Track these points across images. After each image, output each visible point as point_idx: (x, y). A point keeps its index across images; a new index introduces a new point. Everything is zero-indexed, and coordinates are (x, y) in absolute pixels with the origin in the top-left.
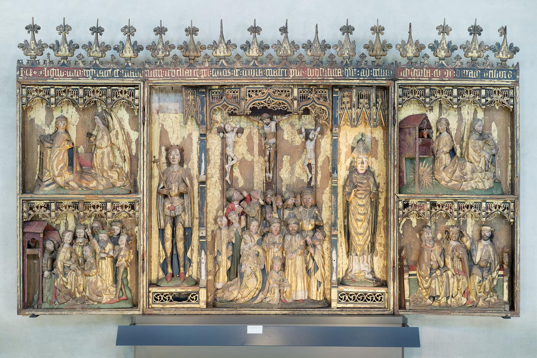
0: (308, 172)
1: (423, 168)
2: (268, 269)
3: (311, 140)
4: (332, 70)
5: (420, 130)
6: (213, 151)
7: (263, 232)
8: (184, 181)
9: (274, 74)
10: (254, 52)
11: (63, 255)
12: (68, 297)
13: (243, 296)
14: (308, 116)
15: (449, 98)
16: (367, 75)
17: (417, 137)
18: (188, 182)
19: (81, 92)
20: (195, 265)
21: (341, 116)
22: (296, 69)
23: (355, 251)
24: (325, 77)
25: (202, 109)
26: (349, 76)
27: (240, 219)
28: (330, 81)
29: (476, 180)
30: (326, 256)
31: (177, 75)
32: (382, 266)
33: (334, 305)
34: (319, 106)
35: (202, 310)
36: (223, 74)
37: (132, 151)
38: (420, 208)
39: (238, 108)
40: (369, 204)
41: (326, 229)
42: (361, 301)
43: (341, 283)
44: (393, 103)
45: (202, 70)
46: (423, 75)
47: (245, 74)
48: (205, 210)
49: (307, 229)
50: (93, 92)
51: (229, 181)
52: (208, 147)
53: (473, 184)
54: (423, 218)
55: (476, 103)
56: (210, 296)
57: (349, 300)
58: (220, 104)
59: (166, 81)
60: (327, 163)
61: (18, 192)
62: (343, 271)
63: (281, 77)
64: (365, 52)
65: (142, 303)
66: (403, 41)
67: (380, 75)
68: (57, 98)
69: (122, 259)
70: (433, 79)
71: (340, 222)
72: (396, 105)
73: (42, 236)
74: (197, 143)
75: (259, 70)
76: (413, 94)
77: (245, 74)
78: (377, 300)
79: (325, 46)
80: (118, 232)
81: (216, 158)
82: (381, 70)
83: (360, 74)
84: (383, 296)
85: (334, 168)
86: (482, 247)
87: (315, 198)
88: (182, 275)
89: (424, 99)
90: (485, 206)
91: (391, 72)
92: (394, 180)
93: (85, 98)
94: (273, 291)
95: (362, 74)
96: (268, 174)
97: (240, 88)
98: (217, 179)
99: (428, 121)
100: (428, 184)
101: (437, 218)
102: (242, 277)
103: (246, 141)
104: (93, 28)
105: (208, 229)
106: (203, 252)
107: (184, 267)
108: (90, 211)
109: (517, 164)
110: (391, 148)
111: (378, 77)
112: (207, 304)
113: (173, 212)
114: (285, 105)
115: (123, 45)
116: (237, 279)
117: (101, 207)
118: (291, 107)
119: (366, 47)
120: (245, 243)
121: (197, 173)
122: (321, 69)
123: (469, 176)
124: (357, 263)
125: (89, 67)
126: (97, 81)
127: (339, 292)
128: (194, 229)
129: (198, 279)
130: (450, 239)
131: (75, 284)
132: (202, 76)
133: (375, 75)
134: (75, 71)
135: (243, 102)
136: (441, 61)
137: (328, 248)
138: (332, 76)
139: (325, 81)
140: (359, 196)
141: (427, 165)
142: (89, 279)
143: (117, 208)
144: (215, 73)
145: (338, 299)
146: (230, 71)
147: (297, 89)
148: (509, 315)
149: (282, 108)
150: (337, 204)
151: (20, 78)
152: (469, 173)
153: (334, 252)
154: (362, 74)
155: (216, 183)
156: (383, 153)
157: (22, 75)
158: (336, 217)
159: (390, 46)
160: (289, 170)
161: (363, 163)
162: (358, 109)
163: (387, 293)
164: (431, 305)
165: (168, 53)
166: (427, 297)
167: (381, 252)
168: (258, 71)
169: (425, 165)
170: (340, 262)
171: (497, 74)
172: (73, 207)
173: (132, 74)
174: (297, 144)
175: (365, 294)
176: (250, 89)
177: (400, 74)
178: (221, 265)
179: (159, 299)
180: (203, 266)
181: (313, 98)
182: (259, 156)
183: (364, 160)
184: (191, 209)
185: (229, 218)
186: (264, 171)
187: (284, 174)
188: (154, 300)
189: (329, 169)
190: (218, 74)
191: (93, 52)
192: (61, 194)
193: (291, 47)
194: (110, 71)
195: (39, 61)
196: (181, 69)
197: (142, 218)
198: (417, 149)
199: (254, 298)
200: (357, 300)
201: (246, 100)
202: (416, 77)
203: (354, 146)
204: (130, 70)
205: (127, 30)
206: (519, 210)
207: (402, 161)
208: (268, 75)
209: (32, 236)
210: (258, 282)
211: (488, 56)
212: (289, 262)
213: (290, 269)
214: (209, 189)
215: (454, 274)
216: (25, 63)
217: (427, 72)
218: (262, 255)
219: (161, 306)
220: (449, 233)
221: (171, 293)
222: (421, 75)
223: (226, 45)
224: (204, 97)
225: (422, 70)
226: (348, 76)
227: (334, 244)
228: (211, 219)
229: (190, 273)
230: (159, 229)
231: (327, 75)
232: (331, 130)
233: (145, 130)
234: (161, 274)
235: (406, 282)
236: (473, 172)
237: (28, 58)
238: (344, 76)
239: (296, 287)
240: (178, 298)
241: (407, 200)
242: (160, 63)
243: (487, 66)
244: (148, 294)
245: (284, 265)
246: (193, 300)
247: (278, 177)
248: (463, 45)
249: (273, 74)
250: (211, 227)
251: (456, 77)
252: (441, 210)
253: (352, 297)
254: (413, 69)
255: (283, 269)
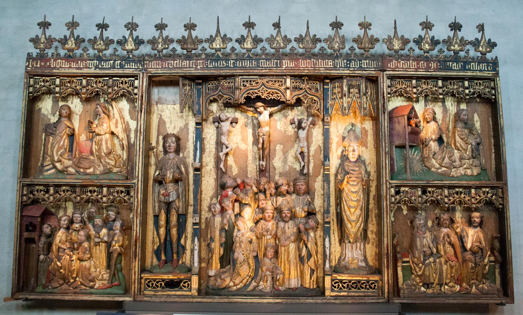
0: (301, 160)
1: (412, 156)
2: (261, 256)
3: (304, 129)
4: (323, 61)
5: (409, 119)
6: (208, 140)
7: (256, 218)
8: (179, 168)
9: (268, 64)
10: (248, 45)
11: (61, 235)
12: (61, 282)
13: (236, 284)
14: (300, 107)
15: (434, 89)
16: (357, 66)
17: (406, 125)
18: (183, 169)
19: (84, 82)
20: (188, 252)
21: (332, 106)
22: (289, 60)
23: (348, 238)
24: (317, 67)
25: (199, 100)
26: (340, 67)
27: (234, 206)
28: (322, 71)
29: (465, 166)
30: (319, 244)
31: (175, 66)
32: (374, 253)
33: (328, 293)
34: (310, 96)
35: (193, 298)
36: (219, 65)
37: (130, 139)
38: (411, 195)
39: (233, 97)
40: (361, 191)
41: (319, 217)
42: (355, 288)
43: (336, 270)
44: (382, 92)
45: (199, 61)
46: (410, 66)
47: (239, 65)
48: (199, 197)
49: (300, 216)
50: (96, 82)
51: (223, 169)
52: (204, 136)
53: (461, 171)
54: (414, 205)
55: (460, 94)
56: (203, 283)
57: (342, 288)
58: (216, 94)
59: (164, 71)
60: (319, 152)
61: (19, 176)
62: (335, 259)
63: (274, 67)
64: (355, 46)
65: (133, 289)
66: (389, 36)
67: (369, 66)
68: (62, 88)
69: (116, 244)
70: (419, 70)
71: (333, 209)
72: (385, 95)
73: (39, 219)
74: (193, 132)
75: (253, 61)
76: (401, 85)
77: (239, 65)
78: (371, 288)
79: (316, 40)
80: (113, 217)
81: (211, 147)
82: (370, 61)
83: (350, 65)
84: (376, 284)
85: (326, 156)
86: (473, 233)
87: (307, 184)
88: (175, 262)
89: (411, 89)
90: (474, 192)
91: (380, 63)
92: (386, 166)
93: (87, 88)
94: (265, 280)
95: (352, 65)
96: (261, 162)
97: (234, 79)
98: (212, 167)
99: (415, 111)
100: (419, 171)
101: (428, 204)
102: (234, 265)
103: (240, 130)
104: (99, 25)
105: (202, 217)
106: (196, 239)
107: (178, 253)
108: (87, 195)
109: (503, 151)
110: (382, 135)
111: (367, 68)
112: (199, 291)
113: (167, 198)
114: (279, 95)
115: (126, 38)
116: (229, 266)
117: (97, 192)
118: (284, 96)
119: (355, 40)
120: (239, 230)
121: (193, 161)
122: (312, 60)
123: (458, 163)
124: (350, 250)
125: (92, 59)
126: (99, 71)
127: (332, 280)
128: (188, 216)
129: (191, 266)
130: (441, 226)
131: (69, 268)
132: (199, 67)
133: (364, 66)
134: (79, 62)
135: (238, 91)
136: (426, 54)
137: (320, 236)
138: (323, 66)
139: (317, 71)
140: (351, 183)
141: (416, 154)
142: (83, 264)
143: (113, 194)
144: (211, 64)
145: (332, 287)
146: (226, 62)
147: (290, 79)
148: (504, 301)
149: (275, 98)
150: (329, 191)
151: (28, 69)
152: (457, 160)
153: (327, 240)
154: (352, 65)
155: (211, 171)
156: (373, 142)
157: (30, 66)
158: (329, 204)
159: (377, 40)
160: (282, 159)
161: (354, 151)
162: (349, 99)
163: (382, 280)
164: (425, 292)
165: (167, 46)
166: (421, 284)
167: (373, 240)
168: (252, 62)
169: (414, 152)
170: (333, 250)
171: (479, 66)
172: (71, 192)
173: (132, 65)
174: (290, 134)
175: (359, 282)
176: (244, 79)
177: (388, 65)
178: (214, 253)
179: (151, 285)
180: (196, 253)
181: (305, 89)
182: (253, 145)
183: (355, 148)
184: (185, 195)
185: (223, 205)
186: (258, 160)
187: (277, 162)
188: (146, 286)
189: (321, 157)
190: (214, 65)
191: (98, 45)
192: (60, 179)
193: (283, 40)
194: (112, 62)
195: (47, 53)
196: (178, 61)
197: (136, 204)
198: (407, 137)
199: (246, 286)
200: (351, 288)
201: (241, 89)
202: (403, 68)
203: (345, 135)
204: (130, 61)
205: (130, 26)
206: (507, 196)
207: (392, 149)
208: (262, 65)
209: (30, 220)
210: (251, 270)
211: (468, 50)
212: (282, 250)
213: (283, 256)
214: (204, 177)
215: (448, 260)
216: (34, 55)
217: (413, 64)
218: (255, 242)
219: (153, 293)
220: (439, 220)
221: (163, 280)
222: (407, 66)
223: (222, 38)
224: (200, 88)
225: (408, 62)
226: (338, 67)
227: (327, 232)
228: (205, 207)
229: (184, 260)
230: (154, 216)
231: (319, 65)
232: (323, 120)
233: (142, 117)
234: (155, 262)
235: (399, 270)
236: (461, 159)
237: (38, 51)
238: (335, 67)
239: (290, 274)
240: (172, 284)
241: (398, 186)
242: (159, 55)
243: (469, 59)
244: (139, 280)
245: (276, 253)
246: (185, 287)
247: (271, 165)
248: (445, 39)
249: (266, 65)
250: (205, 214)
251: (440, 68)
252: (432, 197)
253: (345, 285)
254: (400, 60)
255: (276, 256)
